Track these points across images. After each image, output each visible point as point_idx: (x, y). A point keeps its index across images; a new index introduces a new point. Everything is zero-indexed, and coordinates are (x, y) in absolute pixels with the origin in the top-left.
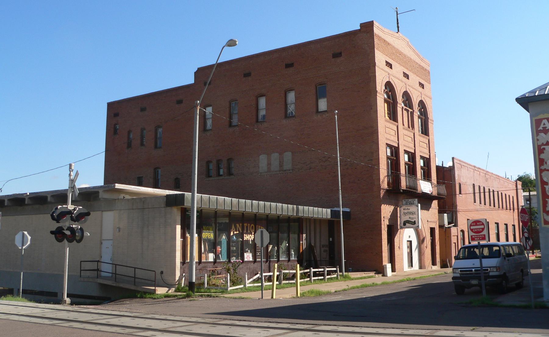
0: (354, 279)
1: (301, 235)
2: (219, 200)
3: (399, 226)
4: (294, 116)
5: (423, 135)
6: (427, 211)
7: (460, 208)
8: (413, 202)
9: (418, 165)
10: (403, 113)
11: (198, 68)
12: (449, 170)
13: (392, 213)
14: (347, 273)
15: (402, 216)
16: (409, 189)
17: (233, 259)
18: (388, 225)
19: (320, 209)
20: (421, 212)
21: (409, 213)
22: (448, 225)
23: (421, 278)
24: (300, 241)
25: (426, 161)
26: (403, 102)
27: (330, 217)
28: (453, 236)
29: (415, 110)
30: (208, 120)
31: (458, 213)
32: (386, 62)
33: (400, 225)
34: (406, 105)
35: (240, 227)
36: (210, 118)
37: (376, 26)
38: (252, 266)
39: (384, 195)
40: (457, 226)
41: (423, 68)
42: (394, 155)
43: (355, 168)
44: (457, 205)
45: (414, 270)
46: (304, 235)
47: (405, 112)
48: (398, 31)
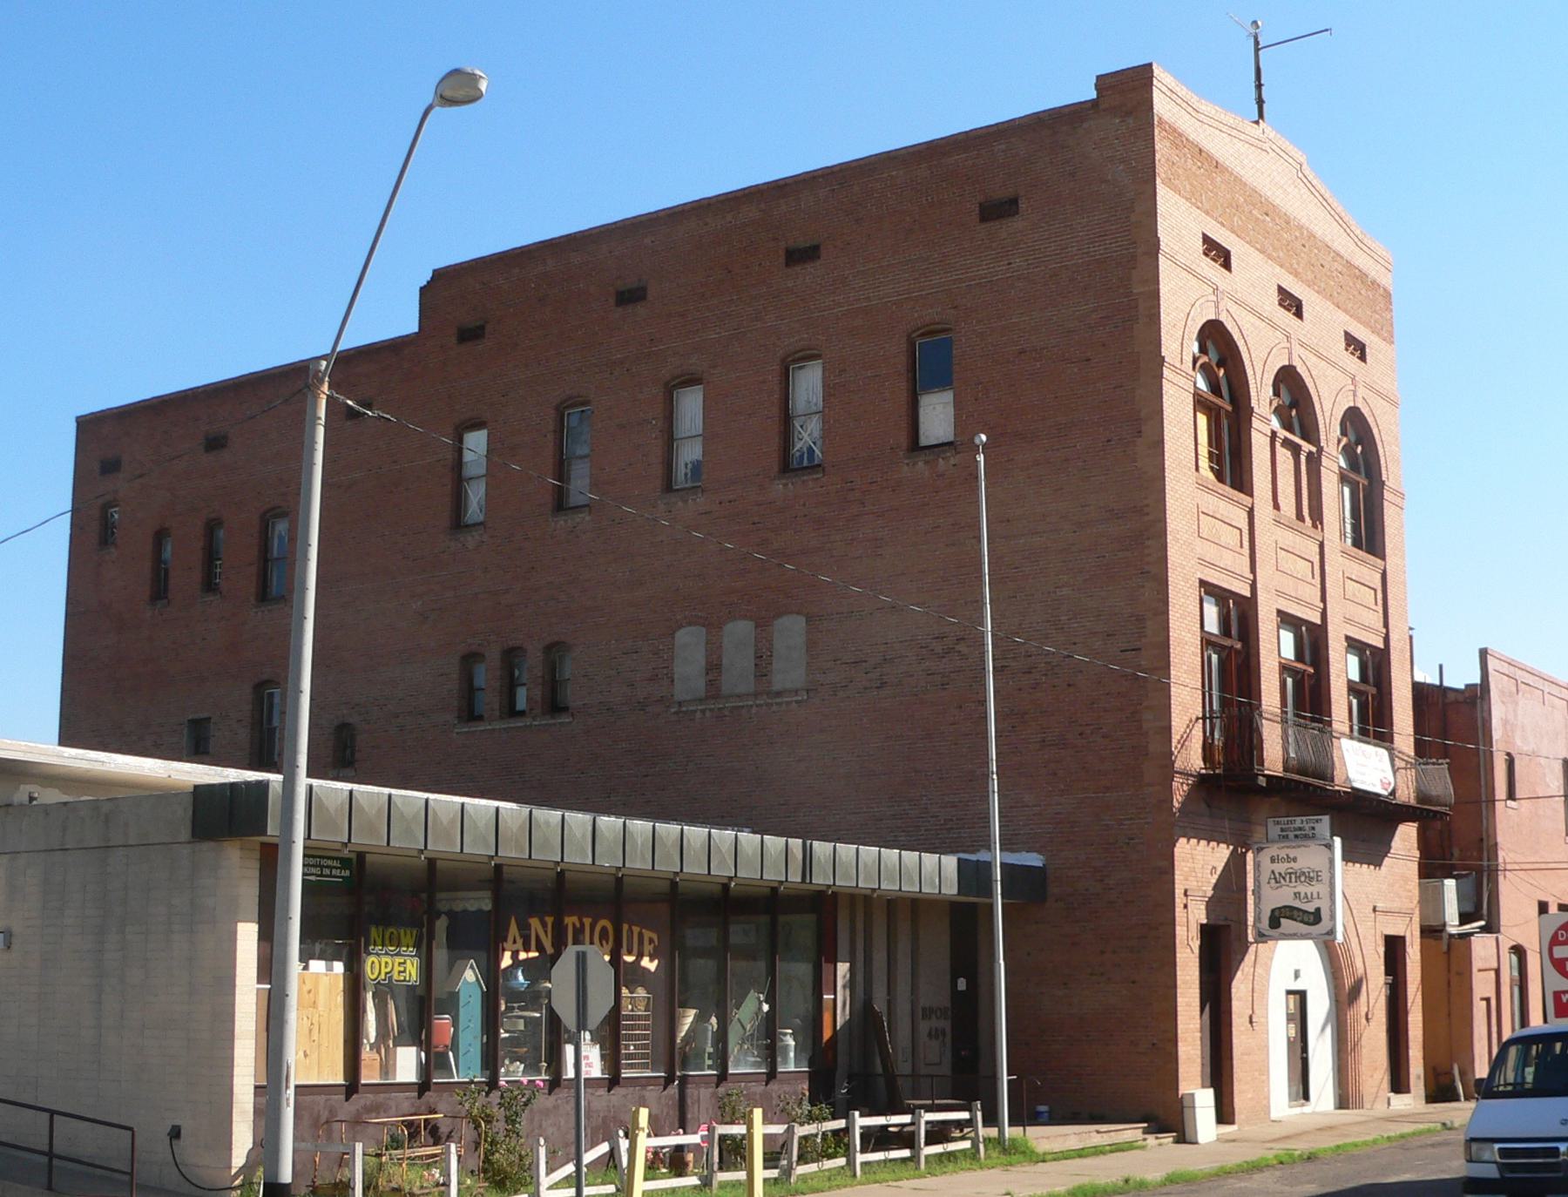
0: (1050, 1157)
1: (826, 967)
2: (435, 813)
3: (1249, 931)
4: (819, 466)
5: (1360, 552)
6: (1372, 867)
7: (1511, 855)
8: (1313, 828)
9: (1338, 676)
10: (1278, 458)
11: (434, 271)
12: (1465, 702)
13: (1220, 876)
14: (1017, 1132)
15: (1266, 891)
16: (1298, 774)
17: (513, 1072)
18: (1202, 925)
19: (910, 857)
20: (1344, 872)
21: (1293, 876)
22: (1462, 924)
23: (1340, 1151)
24: (824, 992)
25: (1373, 663)
26: (1278, 411)
27: (955, 891)
28: (1480, 970)
29: (1325, 449)
30: (471, 482)
31: (1501, 878)
32: (1206, 239)
33: (1254, 926)
34: (1288, 426)
35: (546, 932)
36: (478, 477)
37: (1164, 89)
38: (603, 1100)
39: (1188, 798)
40: (1498, 931)
41: (1362, 276)
42: (1234, 632)
43: (1069, 685)
44: (1496, 844)
45: (1314, 1113)
46: (843, 968)
47: (1284, 455)
48: (1261, 115)
